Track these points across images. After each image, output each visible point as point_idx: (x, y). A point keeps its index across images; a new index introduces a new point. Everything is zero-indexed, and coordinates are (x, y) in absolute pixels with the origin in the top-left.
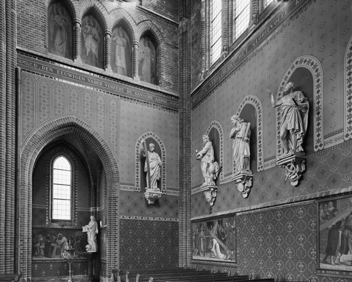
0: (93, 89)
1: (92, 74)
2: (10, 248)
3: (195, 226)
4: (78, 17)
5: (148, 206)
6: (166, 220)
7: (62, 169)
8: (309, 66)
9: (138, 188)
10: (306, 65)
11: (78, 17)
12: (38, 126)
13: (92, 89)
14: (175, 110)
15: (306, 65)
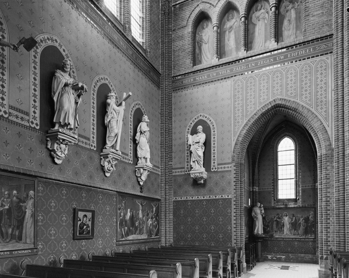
0: (280, 65)
6: (217, 198)
7: (286, 149)
8: (43, 46)
9: (187, 170)
10: (41, 48)
12: (312, 107)
13: (279, 65)
15: (41, 48)
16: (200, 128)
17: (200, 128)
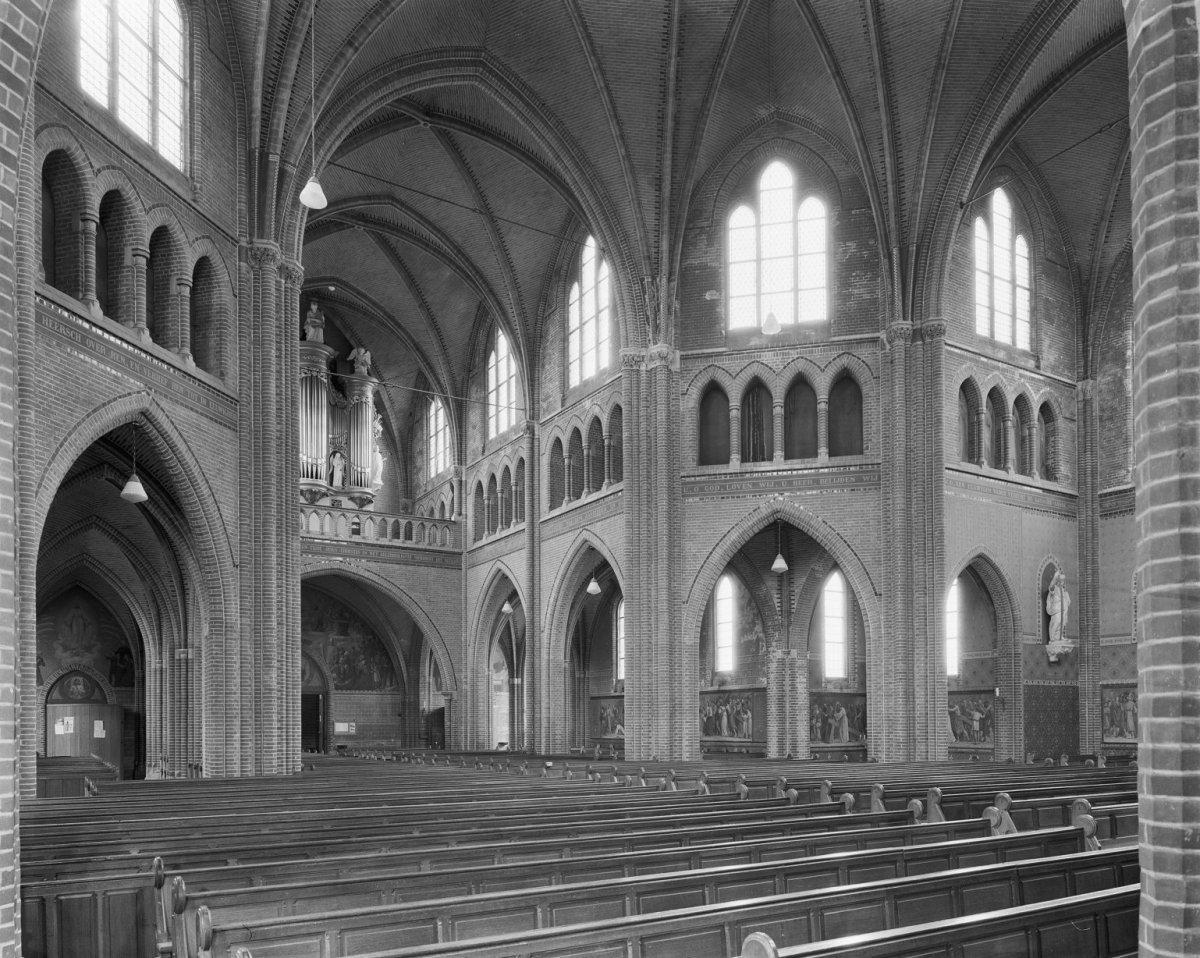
1: (155, 361)
2: (1176, 746)
3: (1109, 694)
4: (89, 208)
5: (1051, 664)
11: (89, 208)
14: (1070, 515)
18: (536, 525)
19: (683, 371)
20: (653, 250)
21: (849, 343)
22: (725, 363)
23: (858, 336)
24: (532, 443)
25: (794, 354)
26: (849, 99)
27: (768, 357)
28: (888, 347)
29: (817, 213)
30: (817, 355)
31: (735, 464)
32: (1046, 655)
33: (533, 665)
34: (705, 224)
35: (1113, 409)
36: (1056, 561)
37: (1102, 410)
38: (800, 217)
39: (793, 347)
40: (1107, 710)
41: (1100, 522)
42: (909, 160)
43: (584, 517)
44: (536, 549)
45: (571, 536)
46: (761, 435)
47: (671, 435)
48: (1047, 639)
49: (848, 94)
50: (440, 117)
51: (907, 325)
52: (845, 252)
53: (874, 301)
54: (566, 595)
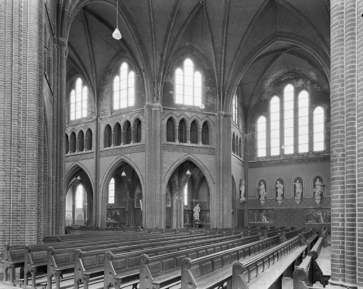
3: (250, 211)
16: (262, 183)
17: (262, 183)
18: (98, 152)
19: (163, 113)
20: (158, 75)
21: (208, 114)
22: (175, 113)
23: (210, 113)
24: (97, 125)
25: (194, 114)
26: (214, 49)
27: (187, 113)
28: (218, 117)
29: (199, 77)
30: (200, 116)
31: (177, 142)
32: (240, 201)
33: (96, 197)
34: (170, 71)
35: (252, 142)
36: (241, 178)
37: (249, 142)
38: (129, 77)
39: (194, 112)
40: (250, 215)
41: (249, 169)
42: (227, 69)
43: (122, 151)
44: (98, 160)
45: (115, 157)
46: (182, 135)
47: (161, 131)
48: (240, 197)
49: (214, 47)
50: (87, 10)
51: (224, 112)
52: (207, 89)
53: (214, 104)
54: (73, 171)
